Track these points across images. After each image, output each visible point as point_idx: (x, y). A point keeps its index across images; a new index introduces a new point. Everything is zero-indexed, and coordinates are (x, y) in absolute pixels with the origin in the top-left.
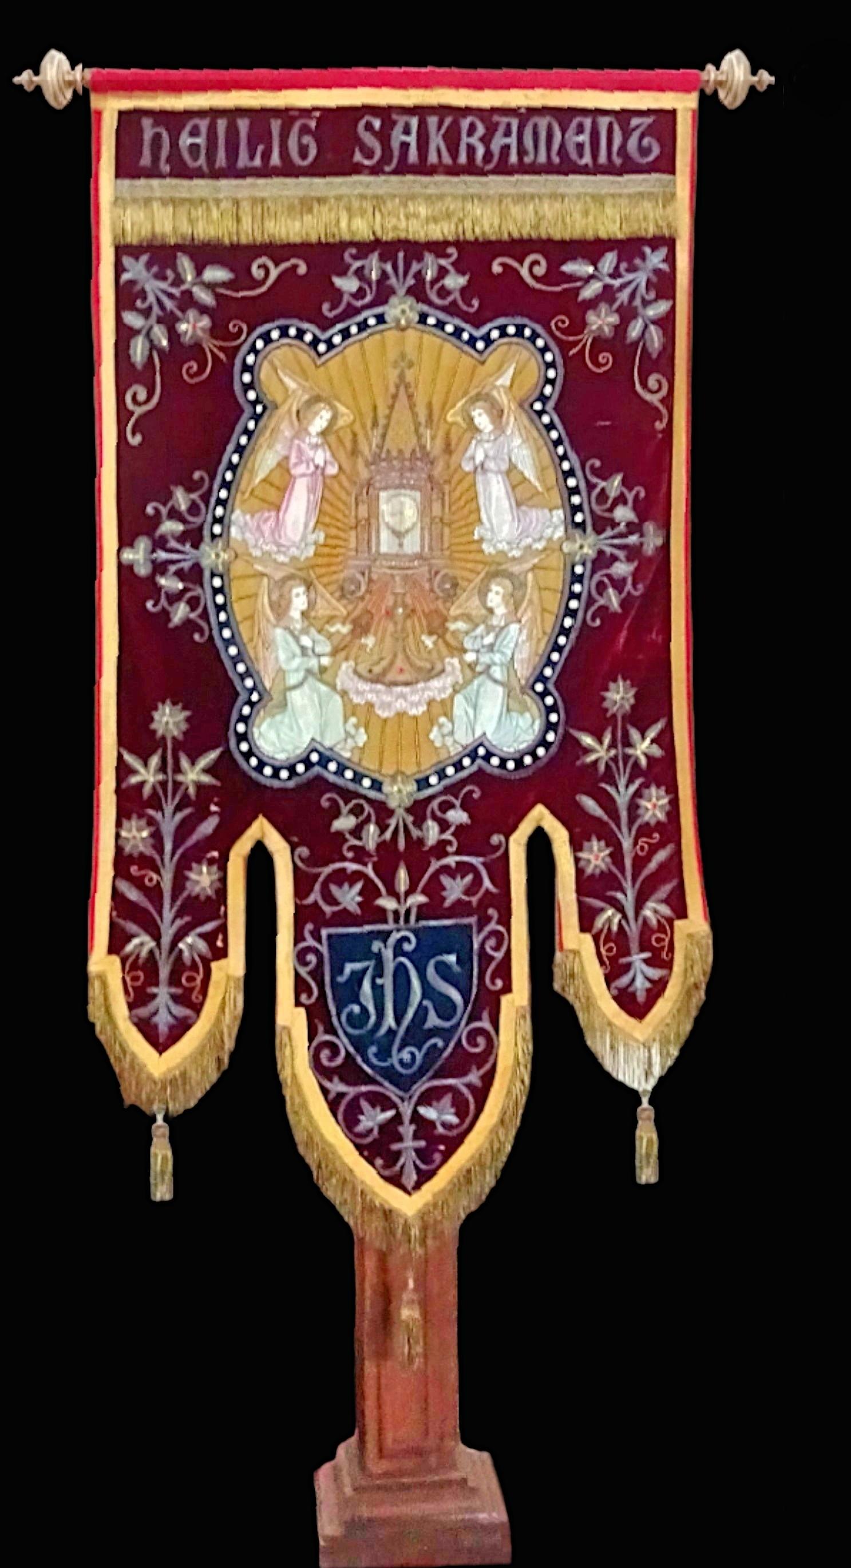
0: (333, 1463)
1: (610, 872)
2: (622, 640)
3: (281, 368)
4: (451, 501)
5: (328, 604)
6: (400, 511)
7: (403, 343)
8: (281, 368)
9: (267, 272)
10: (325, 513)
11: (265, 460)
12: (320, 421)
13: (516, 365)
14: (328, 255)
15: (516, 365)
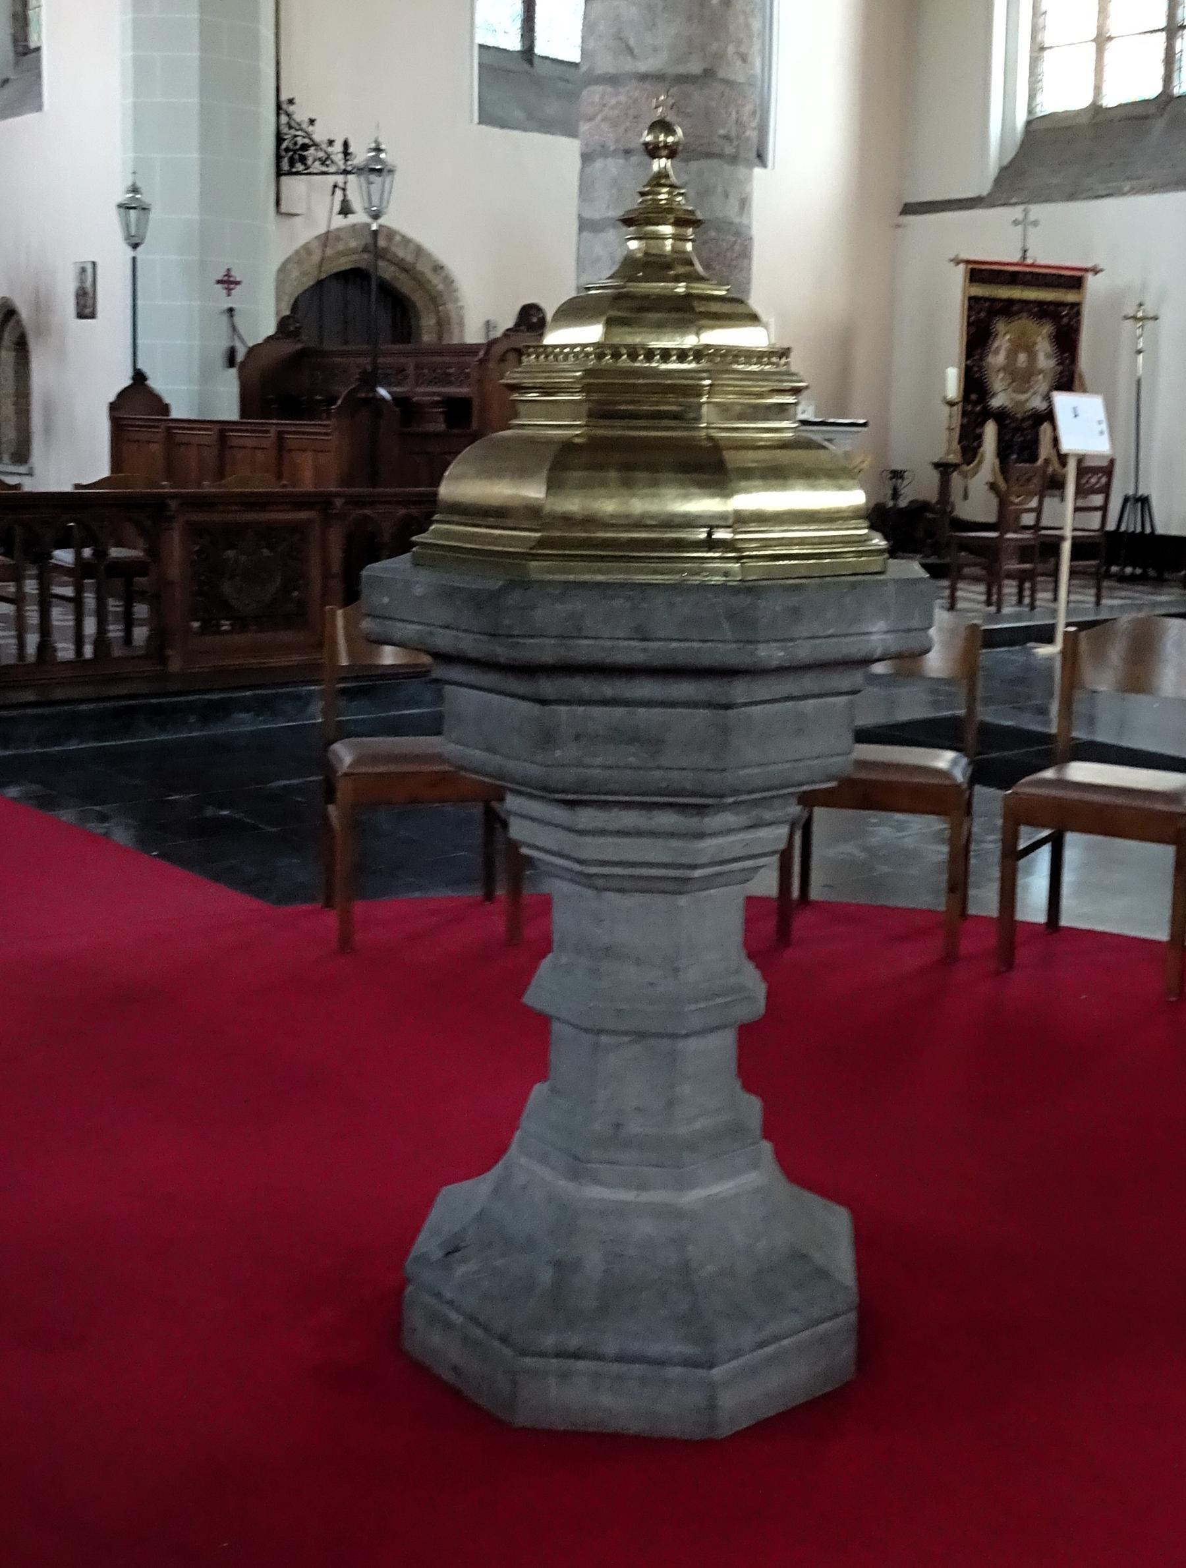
0: (758, 1132)
1: (1050, 669)
2: (993, 755)
3: (1000, 326)
4: (1032, 356)
5: (1008, 376)
6: (1022, 358)
7: (1025, 323)
8: (1000, 326)
9: (999, 305)
10: (1007, 357)
11: (996, 344)
12: (1008, 337)
13: (1047, 329)
14: (1010, 302)
15: (1047, 329)
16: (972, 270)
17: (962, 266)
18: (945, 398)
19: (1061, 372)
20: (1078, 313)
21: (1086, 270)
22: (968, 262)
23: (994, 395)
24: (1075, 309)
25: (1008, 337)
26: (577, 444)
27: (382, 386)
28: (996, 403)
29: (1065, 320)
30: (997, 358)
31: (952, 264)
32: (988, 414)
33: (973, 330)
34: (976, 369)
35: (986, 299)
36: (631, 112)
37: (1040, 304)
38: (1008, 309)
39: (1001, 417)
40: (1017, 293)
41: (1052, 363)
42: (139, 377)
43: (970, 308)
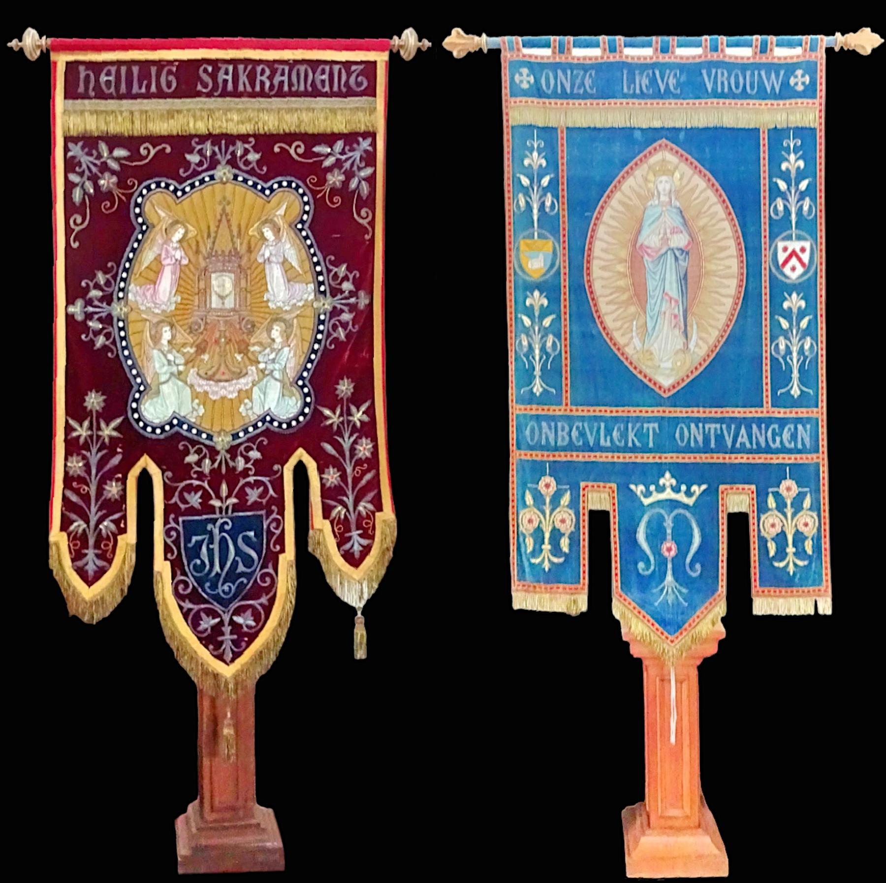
3: (156, 205)
4: (251, 279)
5: (182, 336)
6: (223, 285)
7: (224, 191)
8: (156, 205)
10: (180, 286)
11: (148, 256)
12: (178, 234)
13: (287, 203)
14: (182, 143)
15: (287, 203)
29: (335, 179)
36: (680, 612)
42: (797, 530)
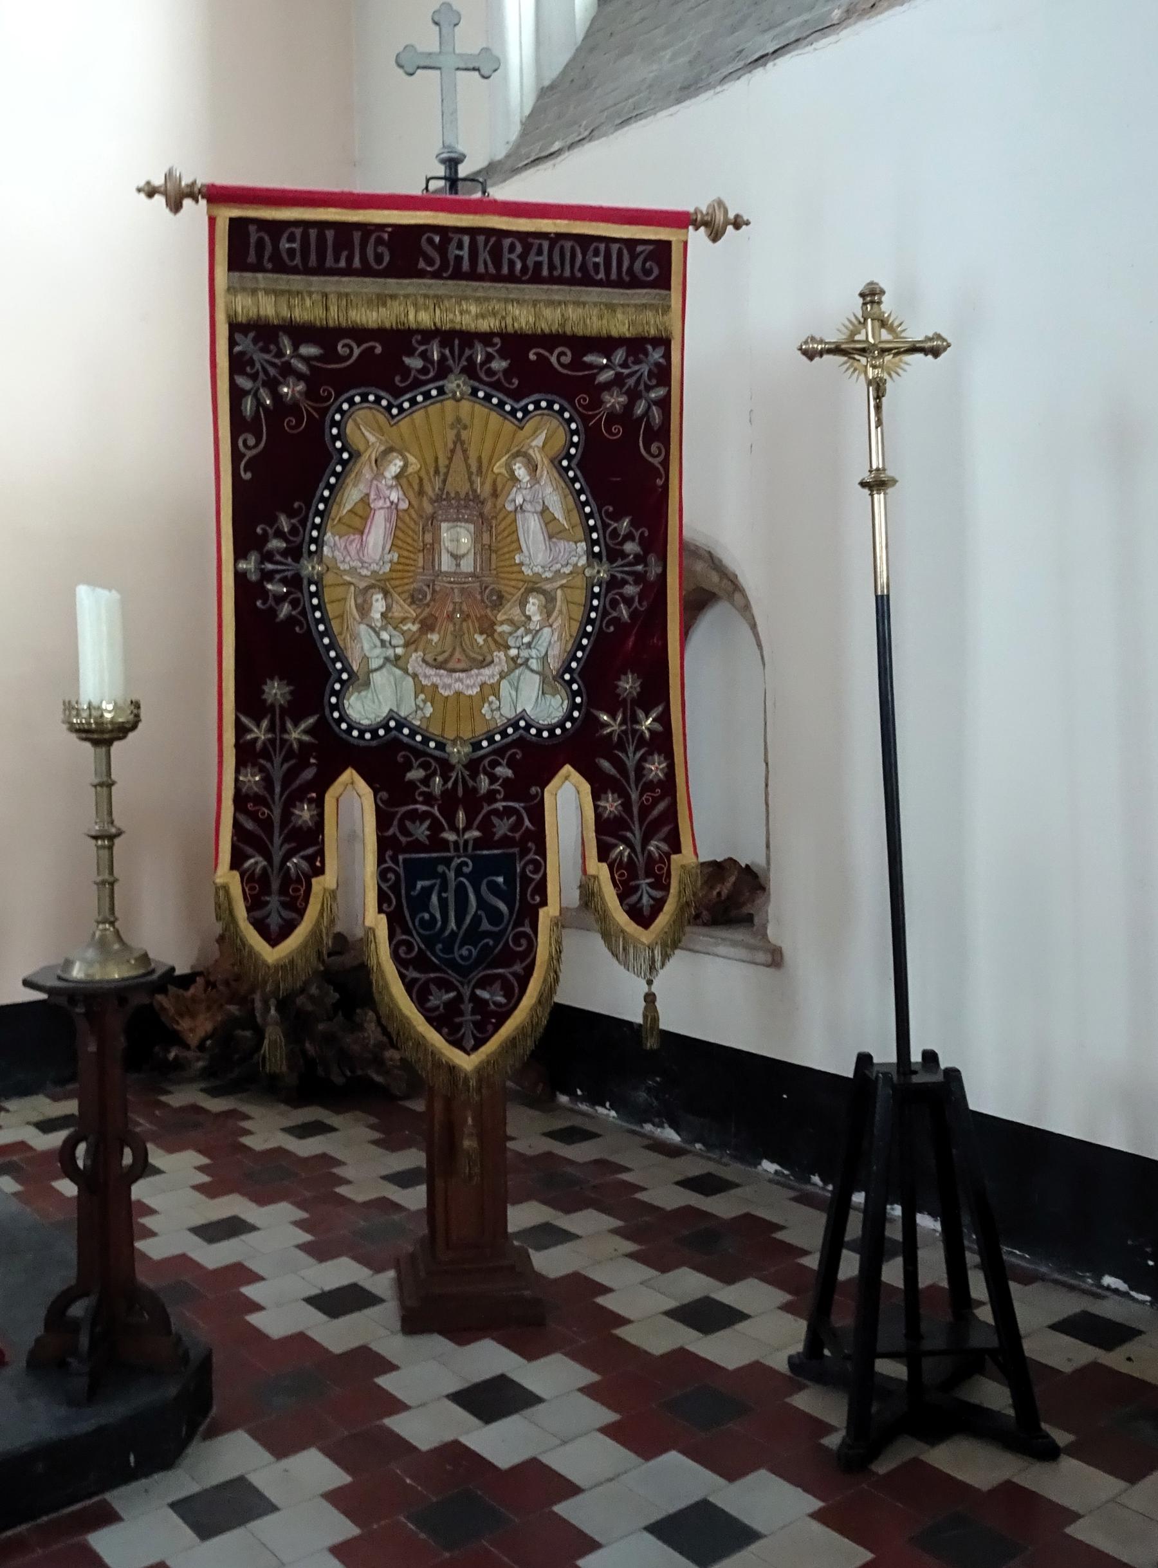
3: (363, 426)
7: (458, 412)
8: (363, 426)
10: (397, 540)
11: (352, 495)
12: (394, 467)
13: (545, 433)
14: (400, 339)
15: (545, 433)
16: (237, 227)
17: (196, 211)
18: (70, 707)
19: (613, 583)
20: (663, 374)
21: (681, 220)
22: (216, 195)
23: (358, 680)
24: (652, 359)
25: (394, 467)
26: (608, 760)
27: (585, 355)
28: (364, 708)
29: (614, 400)
30: (360, 543)
31: (142, 196)
32: (336, 750)
33: (252, 446)
34: (630, 547)
35: (301, 333)
37: (514, 344)
38: (388, 365)
39: (388, 758)
40: (414, 305)
41: (575, 553)
43: (238, 364)
